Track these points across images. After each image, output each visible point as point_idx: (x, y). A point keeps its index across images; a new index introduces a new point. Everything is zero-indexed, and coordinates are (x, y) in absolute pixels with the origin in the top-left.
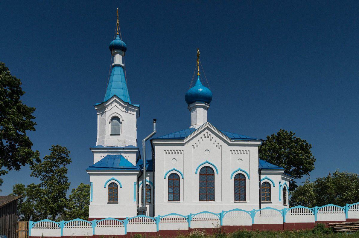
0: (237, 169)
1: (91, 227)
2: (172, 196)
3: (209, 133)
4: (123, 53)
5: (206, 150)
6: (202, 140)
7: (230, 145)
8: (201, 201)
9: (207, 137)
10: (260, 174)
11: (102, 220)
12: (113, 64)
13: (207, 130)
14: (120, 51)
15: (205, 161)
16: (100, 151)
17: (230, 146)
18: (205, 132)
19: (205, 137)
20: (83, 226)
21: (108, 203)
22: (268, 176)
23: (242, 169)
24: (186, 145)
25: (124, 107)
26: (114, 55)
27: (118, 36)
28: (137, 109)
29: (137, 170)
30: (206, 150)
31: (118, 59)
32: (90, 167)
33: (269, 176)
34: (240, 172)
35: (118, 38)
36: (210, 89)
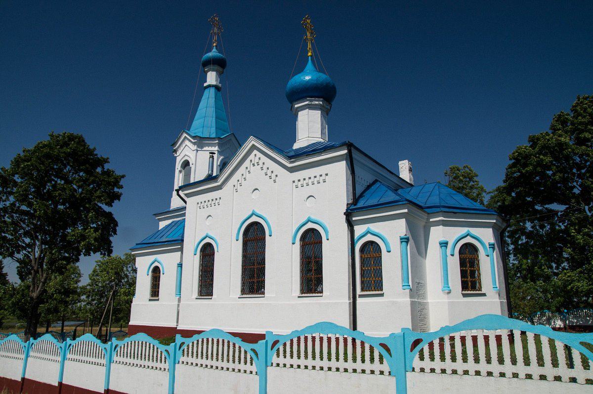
0: (304, 220)
1: (385, 367)
2: (305, 288)
3: (259, 155)
4: (221, 69)
5: (253, 192)
6: (249, 172)
7: (292, 170)
8: (246, 296)
9: (256, 164)
10: (351, 225)
11: (196, 337)
12: (205, 85)
13: (255, 152)
14: (212, 67)
15: (250, 213)
16: (463, 220)
17: (291, 172)
18: (252, 157)
19: (254, 165)
20: (285, 357)
21: (150, 300)
22: (373, 227)
23: (313, 217)
24: (225, 188)
25: (194, 144)
26: (206, 73)
27: (215, 47)
28: (217, 141)
29: (178, 243)
30: (253, 192)
31: (212, 78)
32: (137, 244)
33: (374, 227)
34: (310, 225)
35: (214, 50)
36: (330, 77)
